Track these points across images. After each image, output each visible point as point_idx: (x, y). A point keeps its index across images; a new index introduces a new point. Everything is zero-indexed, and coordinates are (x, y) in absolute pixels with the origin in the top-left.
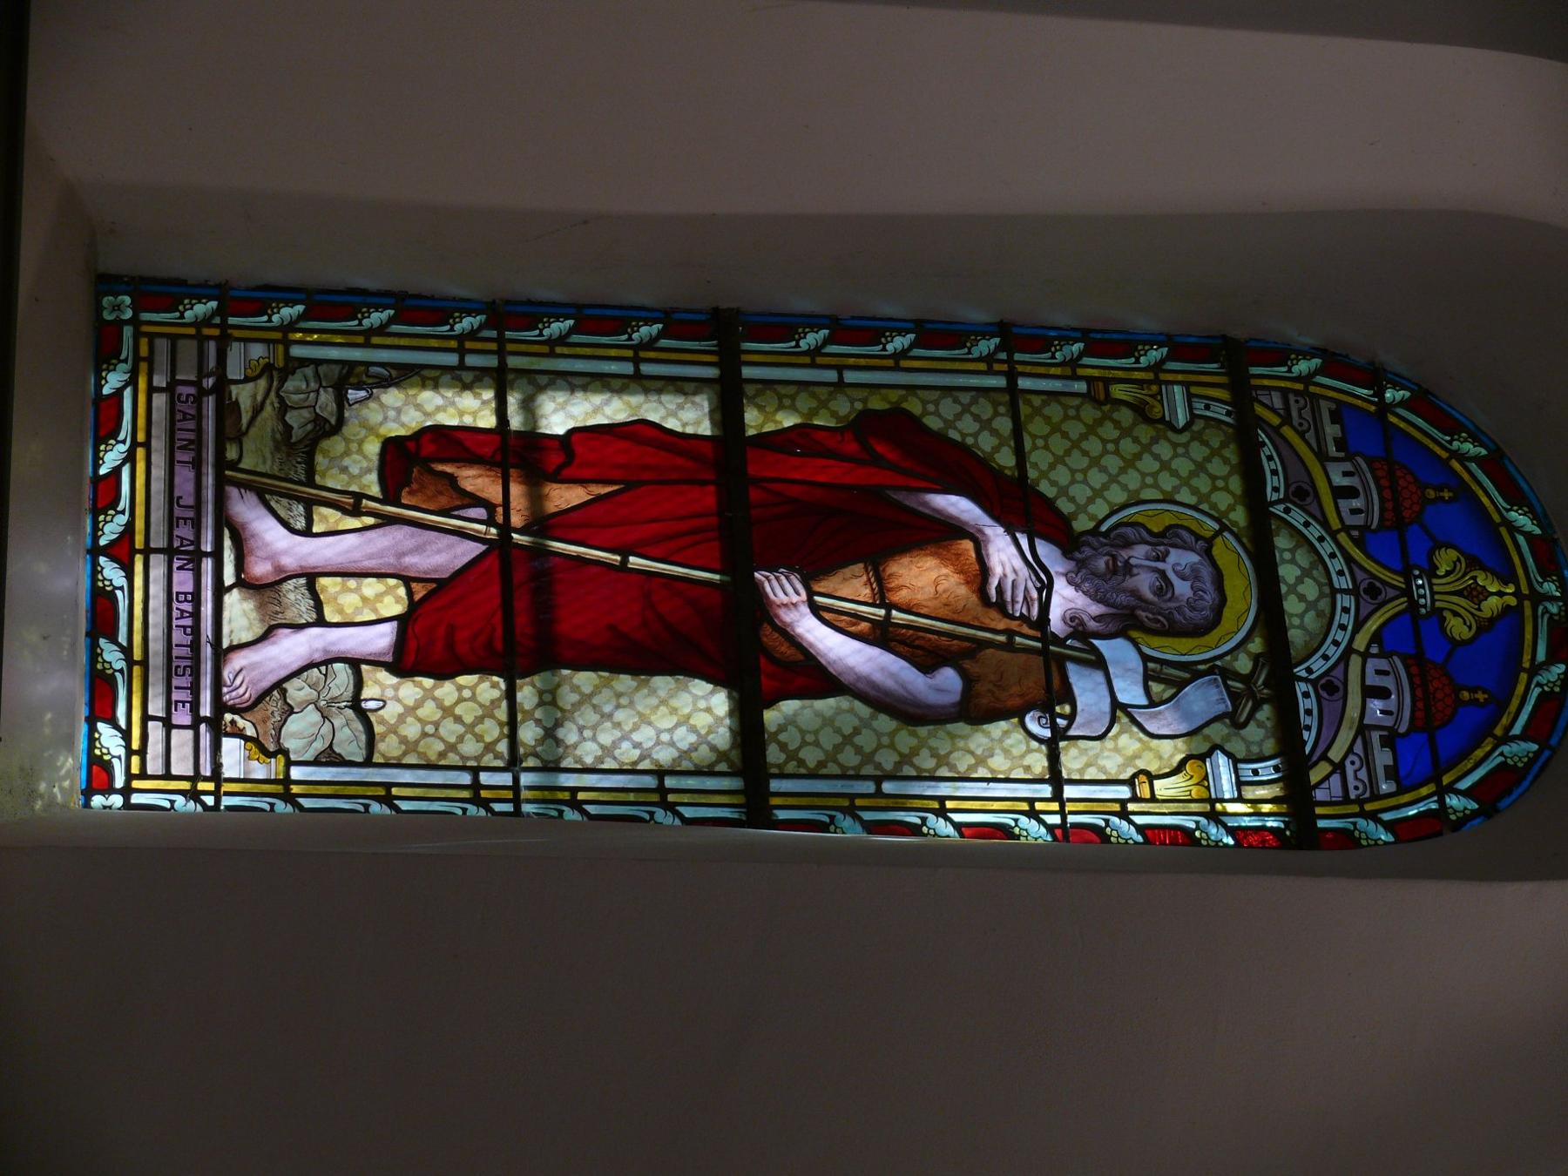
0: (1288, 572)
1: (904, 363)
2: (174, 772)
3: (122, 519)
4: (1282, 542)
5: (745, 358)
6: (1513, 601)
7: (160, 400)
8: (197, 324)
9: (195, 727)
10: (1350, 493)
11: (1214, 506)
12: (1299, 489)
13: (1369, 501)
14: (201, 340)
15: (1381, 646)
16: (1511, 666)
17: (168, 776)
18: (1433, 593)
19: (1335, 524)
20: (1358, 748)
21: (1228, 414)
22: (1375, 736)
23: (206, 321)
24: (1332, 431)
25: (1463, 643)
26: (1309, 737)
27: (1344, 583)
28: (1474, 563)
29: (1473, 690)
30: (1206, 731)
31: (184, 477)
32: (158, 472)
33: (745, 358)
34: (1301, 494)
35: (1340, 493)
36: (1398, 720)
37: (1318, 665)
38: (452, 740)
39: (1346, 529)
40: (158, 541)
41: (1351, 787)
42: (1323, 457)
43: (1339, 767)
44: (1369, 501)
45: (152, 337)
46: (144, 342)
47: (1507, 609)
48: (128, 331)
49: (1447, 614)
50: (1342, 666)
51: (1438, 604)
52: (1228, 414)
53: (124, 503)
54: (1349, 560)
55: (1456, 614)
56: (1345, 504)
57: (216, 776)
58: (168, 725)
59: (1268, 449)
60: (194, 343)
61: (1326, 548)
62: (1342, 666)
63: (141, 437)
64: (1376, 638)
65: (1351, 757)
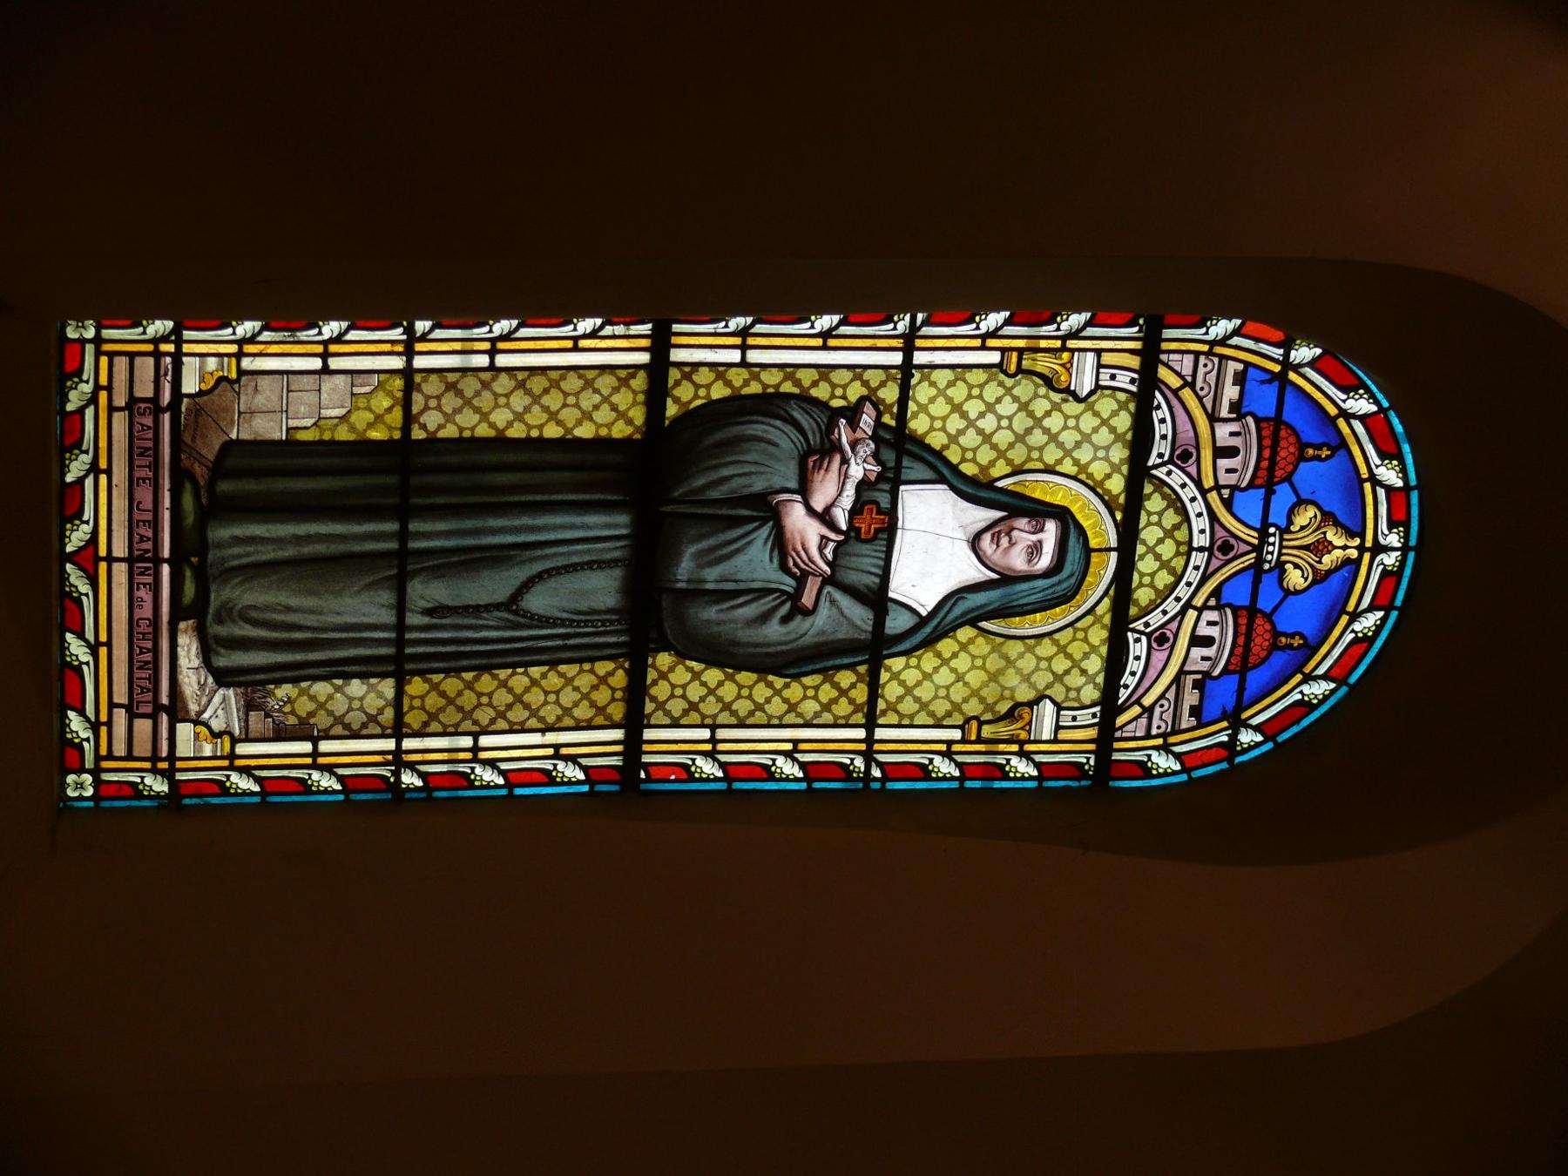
0: (1150, 535)
1: (832, 342)
2: (136, 754)
3: (87, 528)
4: (1155, 503)
5: (674, 340)
6: (1354, 554)
7: (120, 420)
8: (156, 341)
9: (154, 717)
10: (1231, 452)
11: (1090, 476)
12: (1186, 451)
13: (1245, 464)
14: (157, 355)
15: (1218, 600)
16: (1337, 609)
17: (130, 757)
18: (1281, 547)
19: (1208, 482)
20: (1171, 695)
21: (1132, 381)
22: (1190, 679)
23: (165, 339)
24: (1231, 392)
25: (1297, 592)
26: (1129, 680)
27: (1201, 540)
28: (1328, 517)
29: (1290, 647)
30: (1056, 636)
31: (145, 495)
32: (121, 595)
33: (674, 340)
34: (1182, 456)
35: (1221, 452)
36: (1214, 666)
37: (1156, 619)
38: (374, 712)
39: (1218, 487)
40: (120, 550)
41: (1155, 725)
42: (1213, 418)
43: (1149, 711)
44: (1245, 464)
45: (111, 355)
46: (104, 360)
47: (1347, 561)
48: (90, 348)
49: (1289, 567)
50: (1217, 526)
51: (1284, 558)
52: (1132, 381)
53: (88, 514)
54: (1213, 518)
55: (1296, 566)
56: (1224, 463)
57: (172, 758)
58: (132, 715)
59: (1164, 412)
60: (151, 360)
61: (1193, 509)
62: (1217, 526)
63: (103, 381)
64: (1216, 593)
65: (1164, 702)
